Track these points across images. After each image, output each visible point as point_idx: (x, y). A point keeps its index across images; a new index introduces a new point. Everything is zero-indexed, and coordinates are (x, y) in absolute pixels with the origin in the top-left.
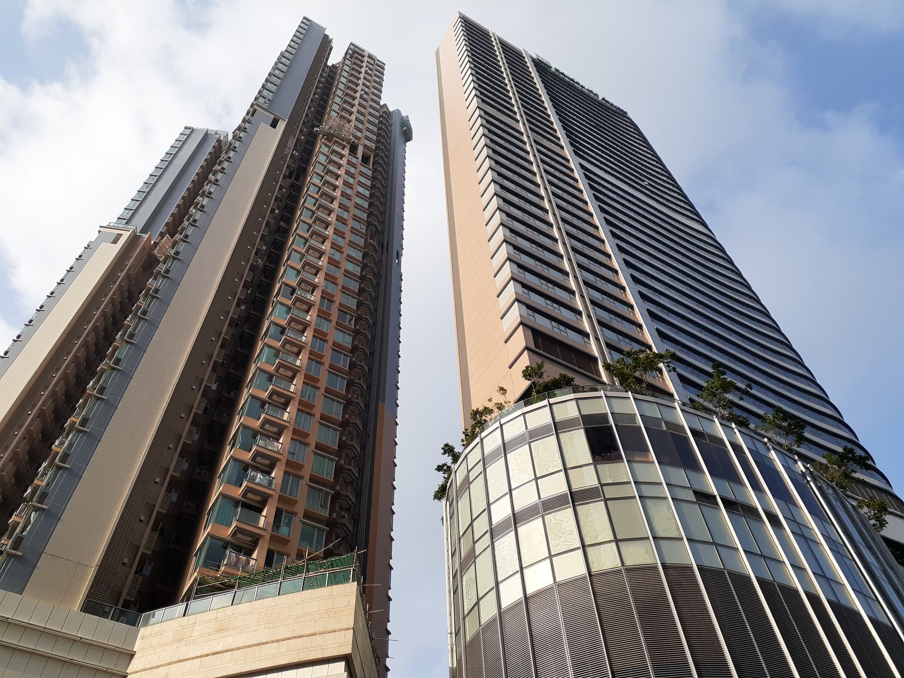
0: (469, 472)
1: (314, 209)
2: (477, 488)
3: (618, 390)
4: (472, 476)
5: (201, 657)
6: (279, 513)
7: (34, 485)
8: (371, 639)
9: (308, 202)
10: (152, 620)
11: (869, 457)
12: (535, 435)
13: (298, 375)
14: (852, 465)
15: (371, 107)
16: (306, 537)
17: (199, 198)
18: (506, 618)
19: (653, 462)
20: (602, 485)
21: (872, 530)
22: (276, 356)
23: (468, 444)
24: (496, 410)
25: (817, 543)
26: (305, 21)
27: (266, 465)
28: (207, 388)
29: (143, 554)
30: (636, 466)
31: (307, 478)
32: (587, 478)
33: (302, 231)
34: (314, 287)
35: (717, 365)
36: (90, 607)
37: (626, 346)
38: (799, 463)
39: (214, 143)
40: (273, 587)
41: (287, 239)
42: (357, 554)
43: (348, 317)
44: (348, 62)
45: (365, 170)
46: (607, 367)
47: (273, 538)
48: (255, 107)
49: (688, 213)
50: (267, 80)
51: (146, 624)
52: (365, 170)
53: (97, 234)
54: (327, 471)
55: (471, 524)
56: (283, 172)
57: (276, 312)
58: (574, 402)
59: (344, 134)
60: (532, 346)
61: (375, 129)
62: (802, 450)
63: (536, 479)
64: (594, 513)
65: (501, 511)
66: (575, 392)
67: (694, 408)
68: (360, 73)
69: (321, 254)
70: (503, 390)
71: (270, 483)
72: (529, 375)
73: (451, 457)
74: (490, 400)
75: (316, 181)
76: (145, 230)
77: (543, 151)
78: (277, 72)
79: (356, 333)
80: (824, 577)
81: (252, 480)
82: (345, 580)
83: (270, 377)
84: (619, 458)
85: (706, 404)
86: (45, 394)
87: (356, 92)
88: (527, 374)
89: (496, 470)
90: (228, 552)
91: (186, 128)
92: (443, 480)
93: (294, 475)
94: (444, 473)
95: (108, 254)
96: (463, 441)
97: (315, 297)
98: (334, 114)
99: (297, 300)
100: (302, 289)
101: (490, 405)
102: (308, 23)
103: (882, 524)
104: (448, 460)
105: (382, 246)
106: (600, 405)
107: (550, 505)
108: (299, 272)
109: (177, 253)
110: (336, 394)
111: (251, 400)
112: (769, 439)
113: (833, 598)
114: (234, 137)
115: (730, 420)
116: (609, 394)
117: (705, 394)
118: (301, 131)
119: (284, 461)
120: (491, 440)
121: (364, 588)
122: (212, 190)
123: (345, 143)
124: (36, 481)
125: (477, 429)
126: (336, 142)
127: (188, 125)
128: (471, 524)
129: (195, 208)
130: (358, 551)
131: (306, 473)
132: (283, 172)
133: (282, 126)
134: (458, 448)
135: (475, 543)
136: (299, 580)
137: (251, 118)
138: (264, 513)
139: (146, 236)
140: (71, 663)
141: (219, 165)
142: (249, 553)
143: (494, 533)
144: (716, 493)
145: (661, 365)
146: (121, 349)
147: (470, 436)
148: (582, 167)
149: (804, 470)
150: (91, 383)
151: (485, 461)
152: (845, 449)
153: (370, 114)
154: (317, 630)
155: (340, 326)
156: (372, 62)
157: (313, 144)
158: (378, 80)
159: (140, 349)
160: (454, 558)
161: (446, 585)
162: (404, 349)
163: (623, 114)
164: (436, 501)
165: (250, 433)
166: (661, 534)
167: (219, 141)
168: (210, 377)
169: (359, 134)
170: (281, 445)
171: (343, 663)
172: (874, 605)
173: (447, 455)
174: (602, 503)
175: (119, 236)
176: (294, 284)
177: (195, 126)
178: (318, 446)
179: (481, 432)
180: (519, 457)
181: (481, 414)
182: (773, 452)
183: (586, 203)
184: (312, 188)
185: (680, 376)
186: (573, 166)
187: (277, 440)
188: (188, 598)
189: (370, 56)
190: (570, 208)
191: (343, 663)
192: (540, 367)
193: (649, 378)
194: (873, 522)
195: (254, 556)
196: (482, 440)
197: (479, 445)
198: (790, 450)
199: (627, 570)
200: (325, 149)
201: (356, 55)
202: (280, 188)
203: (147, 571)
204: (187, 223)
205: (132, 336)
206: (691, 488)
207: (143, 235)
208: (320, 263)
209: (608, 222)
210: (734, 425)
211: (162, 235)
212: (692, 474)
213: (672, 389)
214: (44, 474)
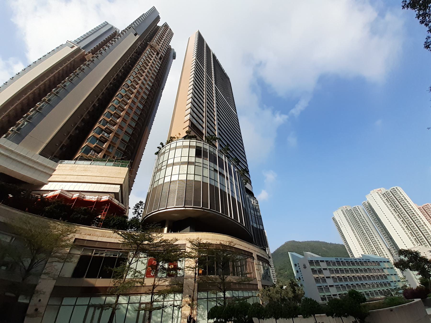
0: (165, 150)
2: (166, 155)
3: (206, 143)
4: (166, 152)
5: (77, 175)
6: (110, 146)
7: (27, 114)
8: (129, 182)
9: (140, 62)
10: (63, 163)
11: (249, 171)
12: (184, 147)
13: (124, 111)
14: (245, 172)
16: (117, 153)
17: (105, 46)
18: (165, 185)
19: (208, 160)
20: (195, 162)
23: (167, 144)
24: (177, 138)
25: (233, 185)
26: (154, 7)
27: (109, 132)
28: (94, 105)
29: (63, 144)
30: (204, 160)
31: (117, 147)
32: (193, 160)
33: (136, 70)
34: (135, 88)
35: (228, 144)
36: (41, 154)
37: (211, 133)
38: (236, 169)
40: (104, 163)
41: (131, 71)
42: (130, 162)
43: (143, 101)
44: (163, 27)
45: (159, 61)
46: (205, 137)
48: (131, 26)
49: (234, 109)
50: (137, 20)
51: (61, 163)
52: (159, 61)
53: (66, 43)
54: (127, 139)
55: (162, 162)
56: (135, 51)
58: (195, 142)
61: (166, 51)
62: (238, 167)
63: (181, 157)
64: (192, 167)
65: (171, 161)
66: (196, 140)
67: (220, 151)
68: (162, 39)
69: (140, 80)
70: (180, 134)
71: (109, 137)
74: (176, 135)
76: (84, 48)
77: (208, 79)
78: (140, 19)
79: (144, 106)
80: (232, 191)
81: (104, 134)
82: (126, 167)
83: (116, 108)
84: (201, 158)
85: (223, 152)
87: (163, 37)
88: (187, 132)
89: (172, 152)
90: (92, 151)
91: (106, 22)
93: (117, 137)
95: (68, 51)
97: (135, 91)
99: (129, 90)
100: (131, 87)
101: (175, 137)
102: (154, 9)
103: (246, 184)
104: (161, 146)
105: (159, 85)
106: (201, 145)
107: (183, 163)
109: (93, 60)
111: (108, 113)
112: (232, 163)
114: (121, 33)
115: (226, 156)
117: (223, 149)
118: (143, 41)
119: (115, 132)
120: (173, 145)
121: (130, 170)
122: (110, 46)
123: (156, 51)
124: (28, 113)
127: (106, 21)
129: (103, 49)
131: (121, 138)
132: (135, 51)
133: (138, 37)
134: (164, 144)
135: (162, 167)
136: (112, 164)
137: (128, 29)
139: (84, 51)
140: (33, 168)
141: (114, 39)
142: (98, 153)
143: (167, 166)
144: (218, 170)
145: (217, 140)
147: (168, 142)
148: (216, 87)
150: (54, 89)
151: (170, 149)
152: (245, 168)
154: (114, 176)
155: (140, 102)
156: (170, 31)
157: (146, 47)
158: (170, 37)
159: (74, 85)
161: (152, 174)
162: (157, 115)
163: (229, 79)
165: (106, 122)
166: (204, 175)
167: (116, 31)
168: (96, 102)
169: (161, 50)
170: (114, 128)
171: (120, 186)
174: (194, 166)
177: (109, 23)
180: (179, 151)
181: (173, 138)
183: (213, 97)
184: (142, 59)
185: (220, 144)
186: (213, 86)
187: (114, 126)
188: (76, 159)
189: (170, 29)
190: (210, 96)
191: (120, 186)
192: (190, 131)
193: (214, 142)
194: (244, 183)
195: (100, 154)
196: (171, 144)
197: (170, 145)
198: (235, 166)
199: (195, 181)
200: (149, 50)
201: (166, 26)
203: (64, 150)
204: (99, 52)
205: (72, 80)
207: (83, 50)
209: (217, 104)
211: (89, 52)
212: (215, 165)
213: (217, 146)
214: (32, 111)
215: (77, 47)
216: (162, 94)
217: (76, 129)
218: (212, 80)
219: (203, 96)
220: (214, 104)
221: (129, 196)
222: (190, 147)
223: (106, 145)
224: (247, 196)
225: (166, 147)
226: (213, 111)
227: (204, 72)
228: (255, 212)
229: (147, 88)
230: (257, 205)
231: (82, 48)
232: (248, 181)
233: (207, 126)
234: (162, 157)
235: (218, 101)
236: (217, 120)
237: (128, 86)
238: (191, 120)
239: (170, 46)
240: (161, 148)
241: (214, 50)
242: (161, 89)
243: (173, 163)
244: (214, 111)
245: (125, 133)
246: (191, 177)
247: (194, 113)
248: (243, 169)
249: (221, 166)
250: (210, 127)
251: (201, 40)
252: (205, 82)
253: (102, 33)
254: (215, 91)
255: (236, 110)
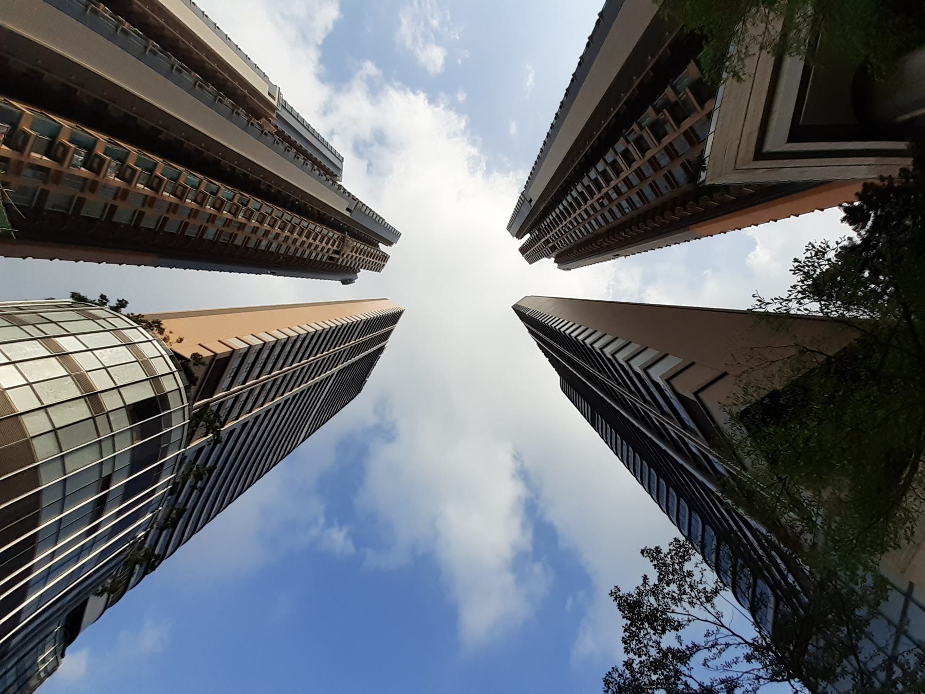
1: (301, 226)
2: (90, 325)
3: (189, 414)
15: (359, 264)
21: (95, 590)
22: (212, 193)
24: (163, 337)
25: (44, 585)
28: (161, 132)
32: (111, 402)
37: (223, 413)
39: (335, 173)
45: (325, 257)
46: (207, 404)
47: (20, 164)
52: (325, 257)
55: (52, 322)
57: (227, 191)
58: (176, 387)
59: (345, 248)
60: (217, 358)
61: (348, 265)
64: (82, 411)
65: (68, 344)
71: (75, 166)
72: (195, 357)
73: (115, 305)
74: (171, 332)
75: (318, 229)
76: (278, 115)
77: (341, 353)
86: (162, 21)
90: (7, 126)
92: (92, 299)
94: (99, 300)
96: (132, 314)
98: (355, 243)
99: (238, 207)
101: (166, 332)
104: (113, 303)
106: (175, 404)
108: (258, 210)
110: (219, 236)
113: (32, 583)
116: (186, 409)
118: (345, 224)
120: (136, 335)
125: (144, 324)
126: (340, 243)
128: (52, 322)
130: (14, 232)
133: (347, 214)
138: (44, 158)
139: (274, 116)
143: (46, 340)
146: (191, 77)
147: (138, 319)
149: (138, 537)
151: (115, 331)
153: (356, 263)
160: (16, 309)
163: (359, 391)
164: (71, 294)
166: (67, 461)
167: (336, 176)
169: (345, 256)
172: (92, 565)
173: (118, 303)
174: (90, 416)
175: (274, 98)
176: (249, 206)
178: (166, 219)
179: (142, 327)
182: (151, 515)
185: (204, 447)
186: (333, 370)
189: (384, 265)
190: (310, 371)
192: (203, 364)
200: (336, 236)
202: (312, 208)
206: (113, 471)
208: (265, 225)
210: (169, 487)
211: (276, 127)
213: (192, 445)
215: (276, 105)
216: (263, 275)
217: (231, 167)
218: (342, 363)
219: (286, 365)
220: (299, 386)
221: (340, 282)
222: (154, 380)
223: (41, 159)
224: (56, 624)
225: (118, 319)
226: (298, 383)
227: (349, 342)
228: (15, 687)
229: (289, 249)
230: (42, 675)
231: (277, 113)
232: (115, 593)
233: (266, 383)
234: (74, 315)
235: (310, 392)
236: (285, 399)
237: (245, 203)
238: (235, 353)
239: (359, 269)
240: (105, 304)
241: (391, 344)
242: (273, 271)
243: (68, 354)
244: (282, 395)
245: (182, 222)
246: (35, 425)
247: (269, 351)
248: (154, 550)
249: (130, 490)
250: (240, 403)
251: (394, 318)
252: (332, 352)
253: (322, 151)
254: (325, 377)
255: (309, 436)
